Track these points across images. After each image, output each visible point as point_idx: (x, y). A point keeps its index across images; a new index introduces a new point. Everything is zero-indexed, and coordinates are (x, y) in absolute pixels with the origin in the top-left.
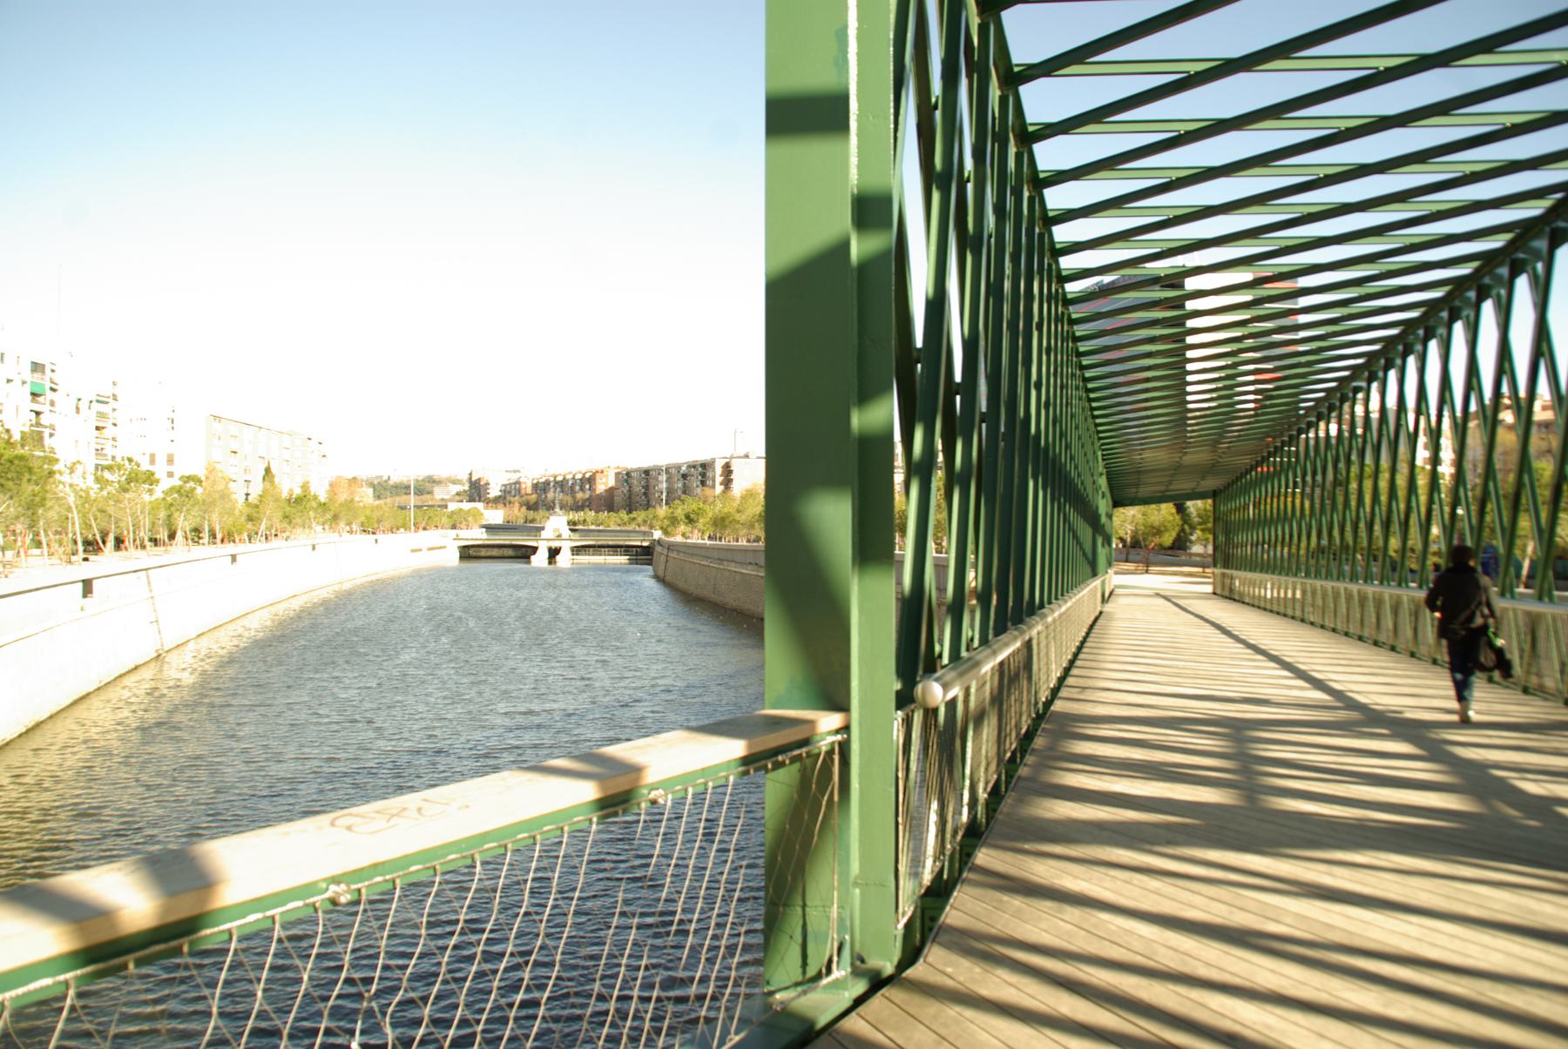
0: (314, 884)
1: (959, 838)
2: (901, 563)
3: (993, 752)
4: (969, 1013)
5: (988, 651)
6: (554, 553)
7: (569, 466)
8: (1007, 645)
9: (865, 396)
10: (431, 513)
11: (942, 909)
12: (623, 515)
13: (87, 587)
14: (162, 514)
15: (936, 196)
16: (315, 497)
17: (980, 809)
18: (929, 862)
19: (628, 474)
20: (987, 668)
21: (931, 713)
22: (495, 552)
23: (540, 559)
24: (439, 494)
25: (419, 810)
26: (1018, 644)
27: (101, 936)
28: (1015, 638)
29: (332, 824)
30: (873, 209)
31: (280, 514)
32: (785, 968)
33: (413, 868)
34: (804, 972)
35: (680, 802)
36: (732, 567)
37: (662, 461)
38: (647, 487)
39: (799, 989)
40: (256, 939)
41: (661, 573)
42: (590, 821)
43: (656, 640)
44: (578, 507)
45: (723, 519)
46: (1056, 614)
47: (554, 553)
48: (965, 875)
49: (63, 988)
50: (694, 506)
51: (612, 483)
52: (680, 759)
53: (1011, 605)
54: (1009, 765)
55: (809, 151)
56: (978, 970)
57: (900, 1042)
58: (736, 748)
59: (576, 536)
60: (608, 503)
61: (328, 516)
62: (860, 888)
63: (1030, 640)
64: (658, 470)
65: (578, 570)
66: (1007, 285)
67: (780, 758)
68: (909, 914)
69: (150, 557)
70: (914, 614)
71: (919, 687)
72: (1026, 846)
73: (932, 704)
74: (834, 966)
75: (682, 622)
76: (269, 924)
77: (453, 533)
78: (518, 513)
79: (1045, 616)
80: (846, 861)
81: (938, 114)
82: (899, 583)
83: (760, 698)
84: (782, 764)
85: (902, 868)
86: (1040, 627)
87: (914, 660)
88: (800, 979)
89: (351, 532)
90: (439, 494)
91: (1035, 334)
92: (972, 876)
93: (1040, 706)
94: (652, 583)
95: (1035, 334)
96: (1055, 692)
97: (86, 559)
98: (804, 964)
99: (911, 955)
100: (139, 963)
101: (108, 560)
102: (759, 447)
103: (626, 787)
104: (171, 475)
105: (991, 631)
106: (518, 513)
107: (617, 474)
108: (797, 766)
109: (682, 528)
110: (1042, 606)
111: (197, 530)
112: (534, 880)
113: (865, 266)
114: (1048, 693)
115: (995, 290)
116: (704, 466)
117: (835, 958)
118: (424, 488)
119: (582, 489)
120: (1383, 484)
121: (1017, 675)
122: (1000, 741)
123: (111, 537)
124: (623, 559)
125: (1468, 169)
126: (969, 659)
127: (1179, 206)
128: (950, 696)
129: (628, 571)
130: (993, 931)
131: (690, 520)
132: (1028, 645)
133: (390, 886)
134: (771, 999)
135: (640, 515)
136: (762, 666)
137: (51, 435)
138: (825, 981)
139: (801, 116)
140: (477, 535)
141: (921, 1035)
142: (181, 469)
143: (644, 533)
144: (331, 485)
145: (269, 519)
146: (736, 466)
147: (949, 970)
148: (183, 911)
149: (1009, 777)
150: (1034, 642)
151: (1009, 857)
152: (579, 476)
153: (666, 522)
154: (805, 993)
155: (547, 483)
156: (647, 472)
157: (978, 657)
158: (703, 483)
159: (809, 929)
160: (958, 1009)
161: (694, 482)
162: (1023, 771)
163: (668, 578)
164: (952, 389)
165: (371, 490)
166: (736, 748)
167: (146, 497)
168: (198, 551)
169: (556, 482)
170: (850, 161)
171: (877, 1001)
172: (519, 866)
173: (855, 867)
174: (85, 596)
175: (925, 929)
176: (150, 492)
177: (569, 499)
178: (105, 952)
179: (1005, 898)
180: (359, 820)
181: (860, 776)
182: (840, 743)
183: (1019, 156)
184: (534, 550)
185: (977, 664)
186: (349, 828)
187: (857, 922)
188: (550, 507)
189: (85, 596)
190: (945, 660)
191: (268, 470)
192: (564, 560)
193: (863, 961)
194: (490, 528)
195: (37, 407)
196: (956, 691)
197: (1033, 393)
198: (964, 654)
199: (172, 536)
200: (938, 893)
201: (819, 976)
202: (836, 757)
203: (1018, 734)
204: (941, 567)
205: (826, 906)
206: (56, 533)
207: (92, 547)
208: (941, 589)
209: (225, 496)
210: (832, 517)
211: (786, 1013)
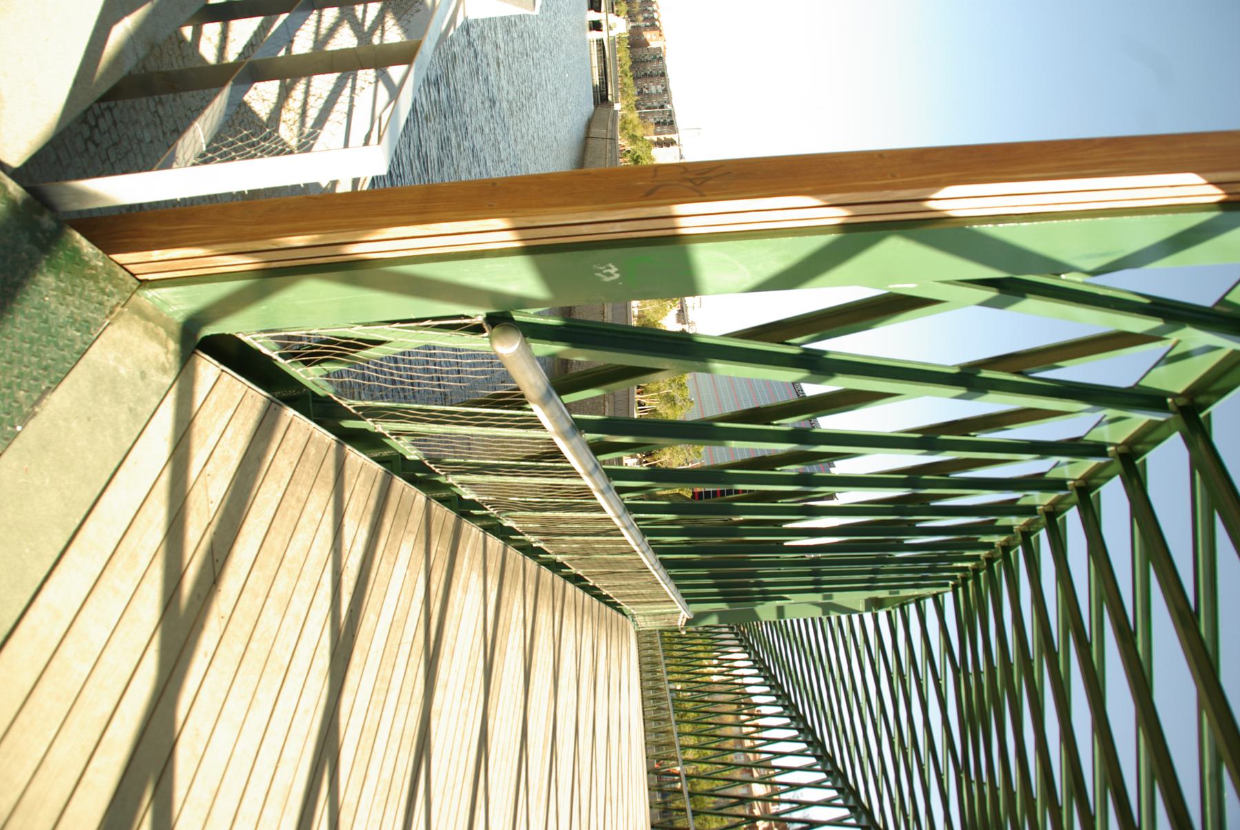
6: (596, 26)
19: (661, 58)
23: (593, 16)
37: (673, 86)
38: (651, 76)
47: (596, 26)
51: (653, 44)
64: (666, 81)
102: (689, 158)
107: (660, 49)
116: (672, 123)
120: (702, 655)
124: (597, 82)
125: (926, 768)
127: (1225, 416)
152: (656, 16)
156: (663, 75)
158: (658, 124)
163: (590, 141)
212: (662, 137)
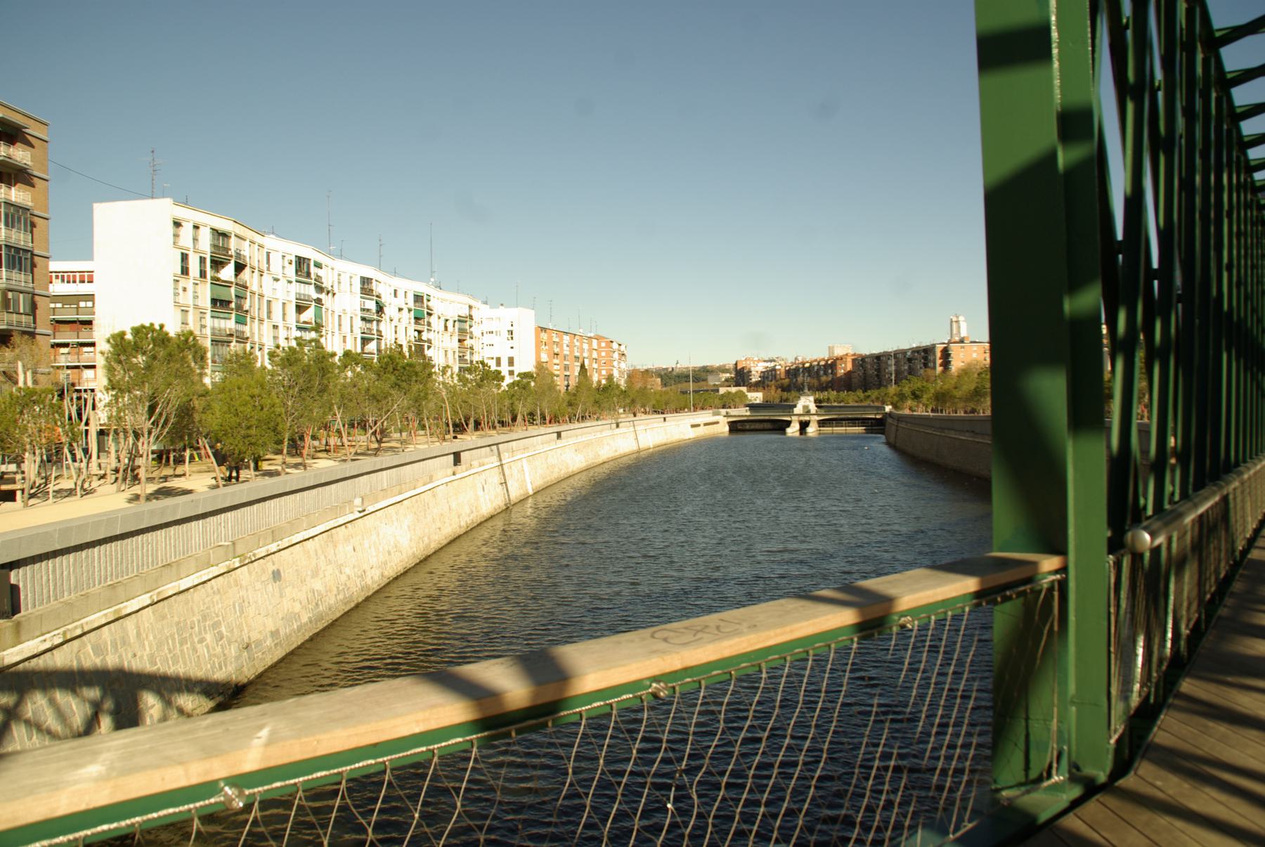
0: (640, 681)
1: (1164, 668)
2: (1109, 429)
3: (1195, 593)
4: (1179, 824)
5: (1189, 504)
6: (804, 425)
7: (812, 351)
8: (1206, 499)
9: (1074, 286)
10: (706, 395)
11: (1149, 729)
12: (860, 393)
13: (457, 458)
14: (507, 402)
15: (1130, 107)
16: (618, 386)
17: (1182, 643)
18: (1137, 687)
20: (1188, 519)
21: (1137, 557)
22: (758, 426)
23: (793, 430)
24: (712, 381)
25: (718, 628)
26: (1217, 498)
27: (493, 711)
28: (1214, 493)
29: (653, 636)
30: (1077, 123)
31: (592, 399)
32: (1009, 771)
33: (715, 673)
34: (1027, 775)
35: (924, 628)
36: (953, 435)
38: (878, 370)
39: (1023, 789)
40: (598, 723)
41: (892, 440)
42: (852, 640)
43: (887, 495)
44: (822, 388)
45: (943, 395)
46: (1252, 472)
47: (804, 425)
48: (1170, 700)
49: (469, 745)
50: (919, 385)
51: (849, 367)
52: (923, 593)
53: (1208, 463)
54: (1209, 606)
55: (1019, 79)
56: (1186, 786)
57: (1114, 842)
58: (969, 584)
59: (822, 411)
60: (847, 383)
61: (628, 401)
62: (1077, 706)
63: (1227, 495)
64: (887, 355)
65: (822, 438)
66: (1198, 179)
67: (1008, 593)
68: (1120, 731)
69: (495, 436)
70: (1121, 470)
71: (1129, 535)
72: (1229, 679)
73: (1139, 548)
74: (1054, 771)
75: (905, 480)
76: (607, 710)
77: (723, 411)
78: (775, 395)
79: (1240, 474)
80: (1064, 683)
81: (1129, 33)
82: (1109, 446)
83: (987, 542)
84: (1010, 598)
85: (1114, 691)
86: (1236, 484)
87: (1122, 514)
88: (1023, 780)
89: (645, 413)
90: (712, 381)
91: (1226, 221)
92: (1177, 702)
93: (1237, 554)
94: (884, 449)
95: (1226, 221)
96: (1251, 542)
97: (455, 437)
98: (1027, 768)
99: (1122, 766)
100: (519, 732)
101: (470, 438)
103: (881, 614)
104: (511, 373)
105: (1190, 487)
106: (775, 395)
107: (854, 360)
108: (1021, 600)
109: (909, 402)
110: (1237, 464)
111: (532, 414)
112: (700, 713)
113: (1071, 172)
114: (1244, 542)
115: (1187, 184)
117: (1055, 765)
118: (701, 374)
119: (826, 373)
121: (1215, 526)
122: (1201, 584)
123: (472, 421)
126: (1172, 511)
128: (1157, 542)
129: (864, 438)
130: (1200, 752)
131: (916, 396)
132: (1225, 499)
133: (697, 685)
134: (998, 796)
135: (874, 393)
136: (989, 515)
137: (429, 347)
138: (1046, 784)
139: (1009, 49)
140: (742, 412)
141: (1133, 837)
142: (518, 369)
143: (878, 408)
144: (629, 376)
145: (584, 403)
146: (955, 351)
147: (1159, 783)
148: (548, 697)
149: (1209, 616)
150: (1231, 497)
151: (1213, 688)
152: (823, 363)
153: (896, 398)
154: (1028, 792)
155: (797, 369)
157: (1182, 509)
158: (926, 365)
159: (1032, 738)
160: (1168, 819)
161: (918, 364)
162: (1223, 611)
164: (1151, 274)
165: (659, 380)
166: (969, 584)
167: (495, 390)
168: (533, 430)
169: (805, 369)
170: (1056, 82)
171: (1092, 806)
172: (796, 676)
173: (1072, 688)
174: (455, 464)
175: (1135, 744)
176: (499, 386)
177: (815, 382)
178: (495, 722)
179: (1211, 724)
180: (672, 634)
181: (1076, 610)
182: (1059, 582)
183: (1206, 62)
184: (788, 423)
185: (1180, 516)
186: (665, 640)
187: (1073, 736)
188: (800, 389)
189: (455, 464)
190: (1150, 512)
191: (582, 366)
192: (812, 430)
193: (1078, 769)
194: (753, 407)
195: (419, 328)
196: (1161, 540)
197: (1225, 274)
198: (1167, 506)
199: (514, 419)
200: (1143, 717)
201: (1040, 779)
202: (1056, 594)
203: (1217, 579)
204: (1144, 432)
205: (1047, 720)
206: (435, 418)
207: (459, 428)
208: (1145, 452)
209: (552, 387)
210: (1050, 390)
211: (1010, 807)
212: (939, 362)
